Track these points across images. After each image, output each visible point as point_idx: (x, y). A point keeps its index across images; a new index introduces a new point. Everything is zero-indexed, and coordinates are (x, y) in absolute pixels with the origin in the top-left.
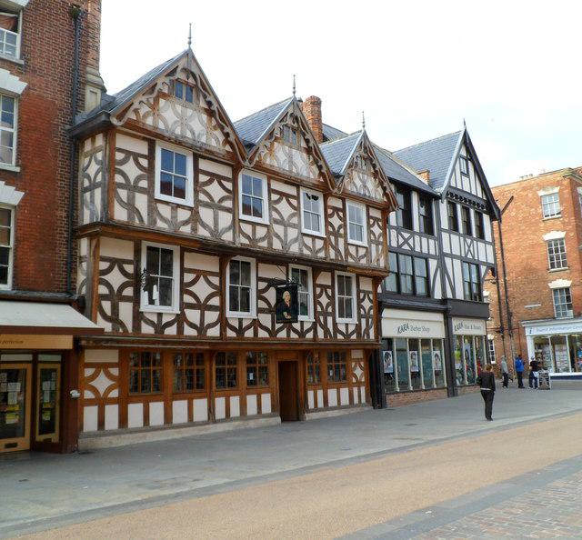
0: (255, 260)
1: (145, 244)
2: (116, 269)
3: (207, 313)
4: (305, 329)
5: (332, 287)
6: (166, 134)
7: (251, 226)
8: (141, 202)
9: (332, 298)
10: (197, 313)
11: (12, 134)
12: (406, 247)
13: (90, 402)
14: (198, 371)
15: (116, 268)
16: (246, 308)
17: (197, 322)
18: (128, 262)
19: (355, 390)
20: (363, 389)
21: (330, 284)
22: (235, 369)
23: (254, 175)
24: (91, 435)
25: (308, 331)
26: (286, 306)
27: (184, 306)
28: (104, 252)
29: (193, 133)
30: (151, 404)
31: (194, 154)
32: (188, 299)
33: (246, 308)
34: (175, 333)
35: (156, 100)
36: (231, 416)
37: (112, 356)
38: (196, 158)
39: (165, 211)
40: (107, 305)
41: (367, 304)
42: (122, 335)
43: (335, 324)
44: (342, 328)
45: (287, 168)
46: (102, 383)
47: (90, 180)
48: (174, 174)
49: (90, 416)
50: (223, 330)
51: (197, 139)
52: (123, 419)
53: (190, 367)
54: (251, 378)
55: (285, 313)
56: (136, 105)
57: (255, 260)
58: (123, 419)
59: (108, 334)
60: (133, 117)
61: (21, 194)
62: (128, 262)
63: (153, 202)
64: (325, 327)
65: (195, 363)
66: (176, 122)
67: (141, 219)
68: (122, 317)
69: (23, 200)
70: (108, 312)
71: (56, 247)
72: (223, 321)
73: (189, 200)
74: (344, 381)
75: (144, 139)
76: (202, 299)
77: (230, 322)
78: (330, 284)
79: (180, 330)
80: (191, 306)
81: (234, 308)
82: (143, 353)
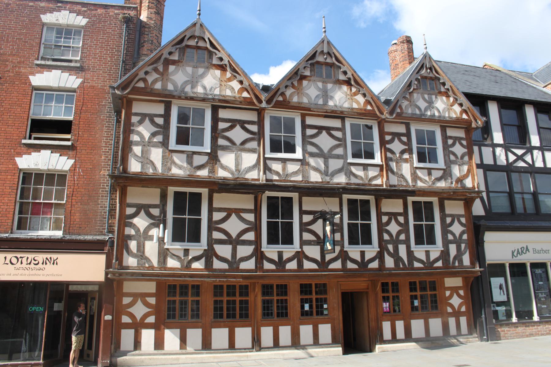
0: (373, 197)
1: (171, 190)
3: (240, 248)
4: (432, 259)
5: (405, 214)
6: (175, 94)
10: (229, 248)
11: (40, 115)
12: (521, 164)
13: (127, 326)
16: (289, 240)
18: (155, 206)
19: (452, 321)
21: (401, 210)
22: (286, 300)
23: (283, 114)
26: (240, 238)
27: (303, 243)
29: (439, 111)
30: (188, 331)
31: (441, 126)
32: (217, 235)
33: (289, 240)
35: (166, 68)
37: (151, 287)
38: (443, 129)
39: (277, 167)
40: (390, 247)
41: (457, 229)
42: (148, 268)
43: (410, 253)
48: (362, 141)
51: (208, 92)
57: (373, 197)
59: (133, 268)
60: (281, 99)
62: (155, 206)
65: (428, 290)
66: (317, 96)
67: (155, 168)
69: (74, 166)
71: (98, 199)
72: (259, 255)
73: (441, 164)
75: (402, 123)
76: (234, 235)
77: (268, 255)
78: (401, 210)
79: (300, 264)
81: (273, 240)
82: (170, 286)
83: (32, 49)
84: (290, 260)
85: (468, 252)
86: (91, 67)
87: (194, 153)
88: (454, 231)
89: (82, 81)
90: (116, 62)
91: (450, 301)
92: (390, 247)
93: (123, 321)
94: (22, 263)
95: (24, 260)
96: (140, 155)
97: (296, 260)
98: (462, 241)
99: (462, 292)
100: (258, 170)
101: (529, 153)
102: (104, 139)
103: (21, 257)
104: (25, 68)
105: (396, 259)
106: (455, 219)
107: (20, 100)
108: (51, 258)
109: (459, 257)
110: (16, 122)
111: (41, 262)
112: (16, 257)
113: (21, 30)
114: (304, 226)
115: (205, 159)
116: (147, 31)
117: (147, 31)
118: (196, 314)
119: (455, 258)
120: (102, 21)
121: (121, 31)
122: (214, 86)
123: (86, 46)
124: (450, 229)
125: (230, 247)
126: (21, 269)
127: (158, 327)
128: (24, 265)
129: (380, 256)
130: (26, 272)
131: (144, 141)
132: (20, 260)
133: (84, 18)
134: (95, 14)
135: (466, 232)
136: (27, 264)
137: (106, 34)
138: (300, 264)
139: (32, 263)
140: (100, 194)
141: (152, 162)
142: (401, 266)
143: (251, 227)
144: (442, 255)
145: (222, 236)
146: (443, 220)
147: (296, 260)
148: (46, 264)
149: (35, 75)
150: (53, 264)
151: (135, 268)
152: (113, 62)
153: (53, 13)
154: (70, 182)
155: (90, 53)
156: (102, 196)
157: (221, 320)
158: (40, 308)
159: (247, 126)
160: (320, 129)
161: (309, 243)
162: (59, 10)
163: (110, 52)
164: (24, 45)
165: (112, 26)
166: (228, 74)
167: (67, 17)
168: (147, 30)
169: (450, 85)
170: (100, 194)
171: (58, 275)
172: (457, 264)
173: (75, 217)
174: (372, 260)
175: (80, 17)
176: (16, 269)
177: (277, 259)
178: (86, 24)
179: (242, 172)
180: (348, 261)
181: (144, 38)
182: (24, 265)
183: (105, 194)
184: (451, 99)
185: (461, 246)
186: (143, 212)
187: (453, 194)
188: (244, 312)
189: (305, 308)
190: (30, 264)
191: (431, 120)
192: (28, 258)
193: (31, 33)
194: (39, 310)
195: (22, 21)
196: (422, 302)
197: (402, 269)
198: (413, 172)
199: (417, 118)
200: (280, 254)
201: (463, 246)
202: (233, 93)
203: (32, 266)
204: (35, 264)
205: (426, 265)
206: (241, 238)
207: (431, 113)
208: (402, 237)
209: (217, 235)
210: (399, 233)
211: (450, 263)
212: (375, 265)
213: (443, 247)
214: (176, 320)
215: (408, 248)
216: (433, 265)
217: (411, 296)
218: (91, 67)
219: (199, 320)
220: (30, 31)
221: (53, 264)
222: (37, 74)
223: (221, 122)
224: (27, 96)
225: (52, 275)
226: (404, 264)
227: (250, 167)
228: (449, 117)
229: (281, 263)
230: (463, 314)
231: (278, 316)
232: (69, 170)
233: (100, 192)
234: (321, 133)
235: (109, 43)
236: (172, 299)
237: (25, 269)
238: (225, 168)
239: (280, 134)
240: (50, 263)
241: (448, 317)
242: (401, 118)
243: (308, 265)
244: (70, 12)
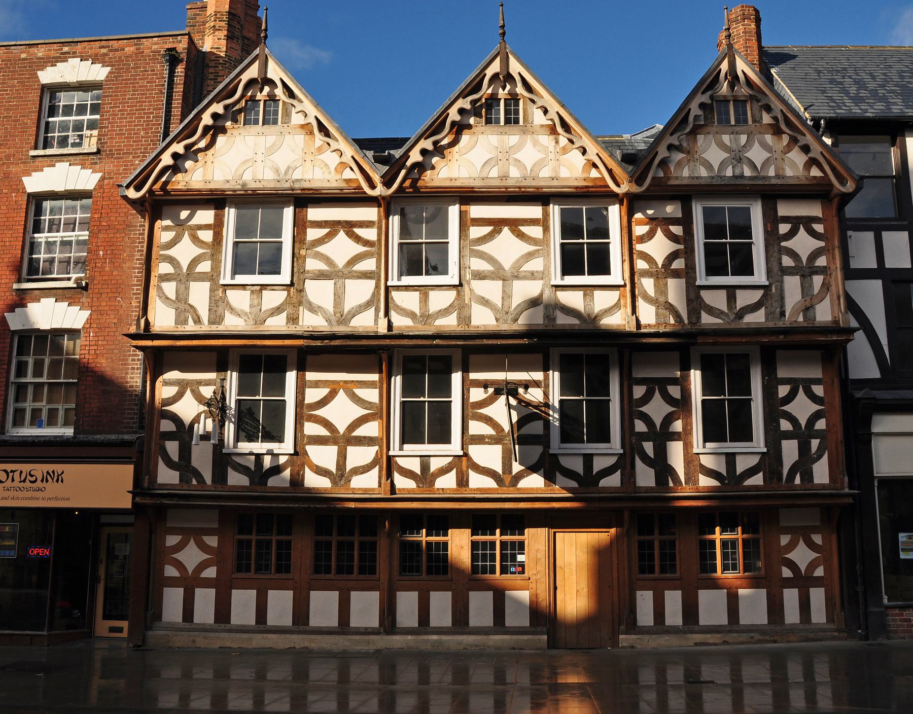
2: (188, 394)
3: (351, 450)
8: (199, 294)
13: (173, 582)
15: (188, 393)
17: (331, 465)
19: (791, 597)
20: (817, 596)
24: (172, 627)
27: (468, 439)
28: (638, 374)
32: (311, 429)
33: (443, 437)
34: (453, 485)
40: (649, 447)
43: (690, 459)
46: (191, 556)
49: (173, 599)
52: (223, 611)
56: (662, 153)
58: (223, 611)
61: (86, 314)
63: (218, 292)
68: (195, 462)
69: (89, 321)
70: (175, 456)
71: (127, 373)
72: (389, 467)
73: (760, 276)
76: (342, 429)
79: (462, 481)
83: (26, 132)
84: (444, 471)
85: (825, 458)
86: (115, 150)
87: (264, 287)
89: (102, 177)
90: (154, 137)
94: (13, 480)
95: (17, 474)
96: (173, 297)
97: (454, 471)
100: (376, 309)
102: (135, 273)
103: (12, 471)
104: (17, 164)
107: (11, 219)
108: (53, 472)
109: (804, 464)
110: (5, 256)
111: (39, 479)
112: (5, 471)
113: (10, 102)
114: (472, 409)
115: (280, 296)
116: (212, 73)
117: (212, 73)
118: (284, 566)
120: (132, 68)
121: (162, 81)
122: (293, 165)
123: (106, 115)
125: (335, 449)
126: (12, 489)
128: (16, 484)
129: (624, 464)
130: (19, 494)
131: (180, 273)
132: (11, 475)
133: (103, 66)
134: (120, 58)
136: (20, 482)
137: (137, 91)
138: (462, 481)
139: (27, 480)
140: (128, 364)
141: (191, 306)
143: (372, 413)
145: (322, 431)
147: (454, 471)
148: (47, 481)
149: (30, 175)
150: (57, 481)
151: (176, 488)
152: (149, 137)
153: (56, 65)
154: (83, 347)
155: (112, 127)
156: (133, 369)
157: (328, 576)
158: (44, 551)
159: (358, 231)
160: (498, 224)
161: (480, 440)
162: (64, 58)
163: (144, 121)
164: (15, 127)
165: (148, 75)
166: (563, 140)
167: (76, 70)
168: (213, 71)
169: (557, 110)
170: (128, 364)
171: (63, 499)
172: (798, 481)
173: (92, 405)
175: (98, 66)
176: (5, 489)
177: (418, 471)
178: (107, 77)
179: (346, 316)
181: (208, 86)
182: (16, 484)
183: (137, 364)
184: (785, 139)
185: (809, 444)
186: (188, 393)
190: (24, 481)
192: (21, 472)
193: (24, 105)
194: (43, 553)
195: (10, 86)
198: (692, 296)
200: (425, 460)
201: (815, 443)
202: (327, 173)
203: (28, 484)
204: (31, 482)
206: (354, 434)
207: (733, 173)
209: (311, 429)
212: (614, 481)
213: (766, 446)
214: (252, 575)
215: (687, 446)
218: (115, 150)
219: (290, 576)
220: (22, 101)
221: (57, 481)
222: (33, 174)
223: (312, 227)
224: (20, 211)
225: (56, 499)
227: (360, 306)
228: (778, 176)
229: (425, 477)
230: (818, 582)
231: (429, 572)
232: (83, 328)
233: (130, 362)
234: (500, 232)
235: (142, 106)
237: (18, 489)
238: (313, 309)
239: (581, 241)
240: (53, 479)
243: (477, 481)
244: (81, 60)
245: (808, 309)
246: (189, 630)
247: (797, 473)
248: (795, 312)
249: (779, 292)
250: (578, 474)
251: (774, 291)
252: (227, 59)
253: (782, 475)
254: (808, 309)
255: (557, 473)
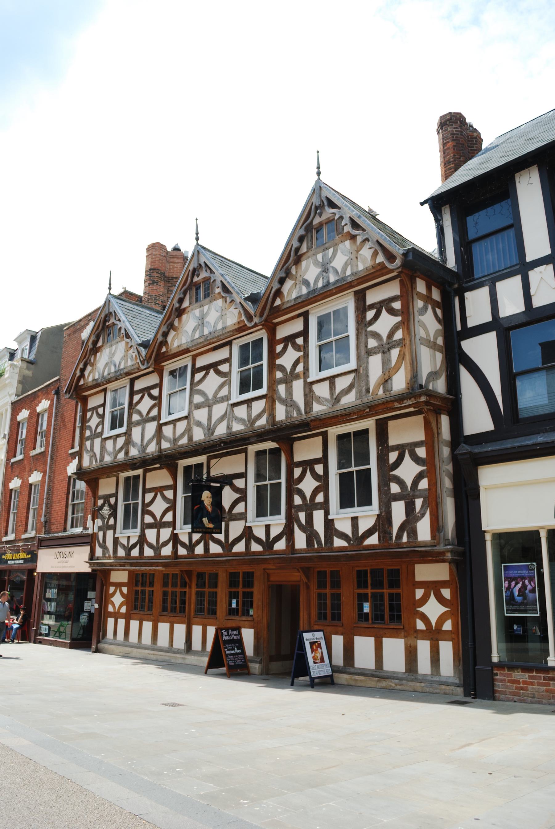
3: (162, 531)
7: (520, 384)
9: (324, 480)
14: (391, 596)
25: (278, 538)
36: (193, 649)
40: (302, 516)
43: (329, 524)
44: (345, 527)
45: (27, 358)
47: (91, 431)
50: (175, 548)
53: (183, 590)
54: (234, 605)
55: (205, 520)
64: (308, 528)
65: (170, 585)
74: (149, 612)
80: (150, 526)
85: (428, 515)
88: (402, 477)
91: (422, 609)
92: (302, 516)
93: (125, 612)
98: (417, 493)
99: (446, 593)
101: (229, 346)
105: (309, 535)
106: (405, 452)
119: (402, 528)
124: (395, 472)
127: (128, 618)
129: (288, 532)
135: (425, 474)
142: (316, 546)
144: (379, 524)
146: (382, 458)
172: (405, 539)
174: (278, 538)
180: (252, 541)
185: (413, 503)
187: (370, 411)
188: (336, 612)
189: (364, 608)
191: (325, 294)
196: (374, 607)
197: (317, 551)
199: (303, 302)
201: (419, 503)
205: (352, 542)
208: (320, 498)
210: (315, 493)
211: (391, 538)
212: (281, 545)
215: (327, 513)
216: (363, 542)
217: (359, 595)
226: (319, 543)
236: (362, 591)
241: (417, 638)
242: (283, 312)
245: (386, 381)
246: (126, 646)
247: (404, 532)
248: (377, 387)
249: (365, 372)
250: (221, 541)
251: (361, 372)
252: (149, 298)
253: (392, 534)
254: (386, 381)
255: (252, 541)
